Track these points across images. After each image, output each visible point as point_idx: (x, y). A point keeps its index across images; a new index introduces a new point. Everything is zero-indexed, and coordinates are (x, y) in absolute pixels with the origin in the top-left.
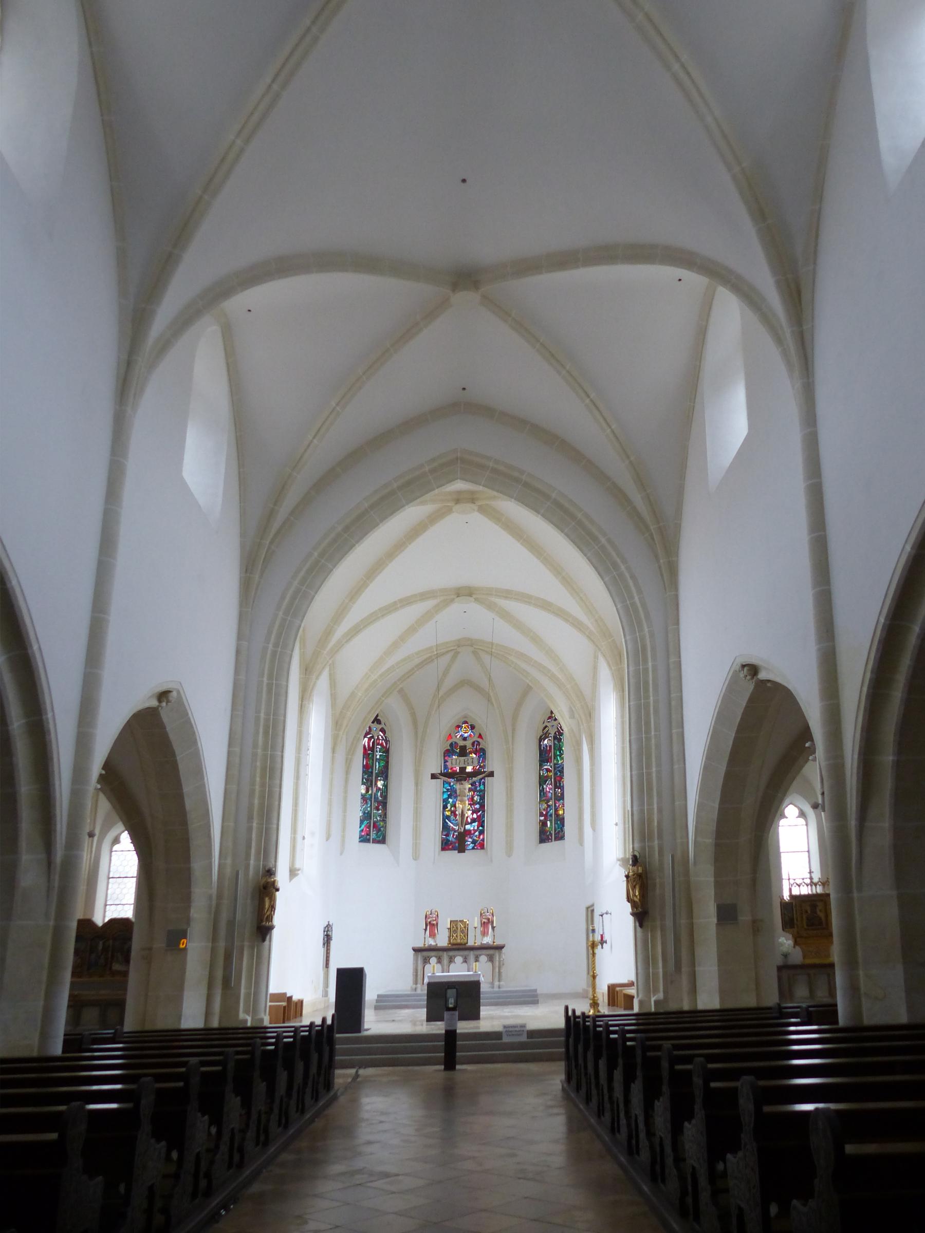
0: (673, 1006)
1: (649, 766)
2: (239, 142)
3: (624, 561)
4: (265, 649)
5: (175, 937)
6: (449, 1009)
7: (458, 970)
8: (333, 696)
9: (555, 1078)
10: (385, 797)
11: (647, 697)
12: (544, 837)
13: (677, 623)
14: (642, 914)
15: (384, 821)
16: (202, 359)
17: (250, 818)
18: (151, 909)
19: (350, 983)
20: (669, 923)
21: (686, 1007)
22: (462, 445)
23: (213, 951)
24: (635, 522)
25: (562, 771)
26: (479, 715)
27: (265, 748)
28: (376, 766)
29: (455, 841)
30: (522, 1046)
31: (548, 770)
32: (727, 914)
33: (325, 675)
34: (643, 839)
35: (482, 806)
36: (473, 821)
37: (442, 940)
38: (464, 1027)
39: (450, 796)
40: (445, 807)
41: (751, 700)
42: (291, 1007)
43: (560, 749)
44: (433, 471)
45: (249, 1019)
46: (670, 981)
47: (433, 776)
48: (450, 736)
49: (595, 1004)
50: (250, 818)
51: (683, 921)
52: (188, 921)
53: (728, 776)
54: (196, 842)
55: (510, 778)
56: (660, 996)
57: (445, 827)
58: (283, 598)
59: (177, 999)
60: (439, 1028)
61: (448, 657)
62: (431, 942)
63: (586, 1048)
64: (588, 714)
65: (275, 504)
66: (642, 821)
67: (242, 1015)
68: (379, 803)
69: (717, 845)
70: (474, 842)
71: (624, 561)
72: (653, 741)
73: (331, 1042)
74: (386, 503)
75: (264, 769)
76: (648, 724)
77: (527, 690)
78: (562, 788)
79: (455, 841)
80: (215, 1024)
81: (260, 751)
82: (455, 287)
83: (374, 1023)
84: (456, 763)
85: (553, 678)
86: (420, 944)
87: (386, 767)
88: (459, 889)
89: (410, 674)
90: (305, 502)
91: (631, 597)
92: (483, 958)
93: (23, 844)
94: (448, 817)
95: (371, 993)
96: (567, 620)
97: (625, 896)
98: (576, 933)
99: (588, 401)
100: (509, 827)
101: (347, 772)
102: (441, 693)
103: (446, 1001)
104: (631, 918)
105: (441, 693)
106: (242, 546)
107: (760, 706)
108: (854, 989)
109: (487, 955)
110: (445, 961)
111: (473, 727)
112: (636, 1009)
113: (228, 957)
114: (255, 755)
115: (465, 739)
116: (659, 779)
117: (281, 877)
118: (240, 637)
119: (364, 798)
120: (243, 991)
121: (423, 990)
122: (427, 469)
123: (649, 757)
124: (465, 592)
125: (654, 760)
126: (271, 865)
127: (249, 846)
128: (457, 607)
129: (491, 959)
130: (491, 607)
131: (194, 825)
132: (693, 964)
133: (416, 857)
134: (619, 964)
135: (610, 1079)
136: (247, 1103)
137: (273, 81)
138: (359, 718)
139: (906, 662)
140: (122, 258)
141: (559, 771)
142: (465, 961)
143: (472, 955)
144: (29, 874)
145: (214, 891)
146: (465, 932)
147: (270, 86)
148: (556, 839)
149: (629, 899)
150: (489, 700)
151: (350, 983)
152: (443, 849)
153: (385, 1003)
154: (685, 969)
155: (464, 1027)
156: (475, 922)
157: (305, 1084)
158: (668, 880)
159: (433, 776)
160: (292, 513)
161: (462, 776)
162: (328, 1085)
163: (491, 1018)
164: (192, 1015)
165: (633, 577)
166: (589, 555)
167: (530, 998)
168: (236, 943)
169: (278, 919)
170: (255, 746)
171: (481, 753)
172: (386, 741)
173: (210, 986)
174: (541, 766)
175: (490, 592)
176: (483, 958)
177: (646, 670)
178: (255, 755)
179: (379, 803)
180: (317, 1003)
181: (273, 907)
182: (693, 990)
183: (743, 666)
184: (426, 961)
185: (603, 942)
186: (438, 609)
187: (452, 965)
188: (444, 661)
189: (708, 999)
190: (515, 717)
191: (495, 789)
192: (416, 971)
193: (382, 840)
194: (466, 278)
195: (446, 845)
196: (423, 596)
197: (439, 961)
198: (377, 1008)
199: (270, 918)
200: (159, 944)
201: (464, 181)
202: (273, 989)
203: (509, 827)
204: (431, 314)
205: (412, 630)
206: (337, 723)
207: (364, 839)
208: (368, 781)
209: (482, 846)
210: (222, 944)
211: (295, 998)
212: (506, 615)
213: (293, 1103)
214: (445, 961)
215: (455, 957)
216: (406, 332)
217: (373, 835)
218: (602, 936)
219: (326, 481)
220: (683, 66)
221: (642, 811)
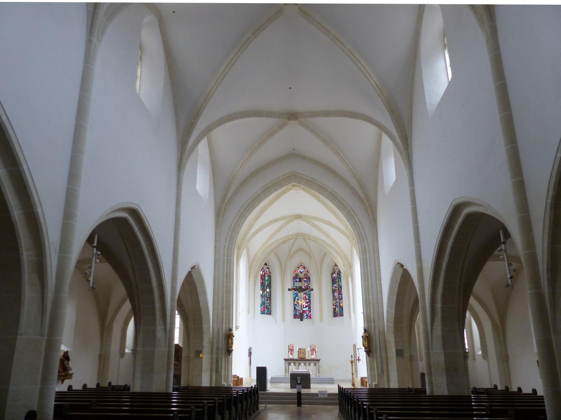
0: (381, 387)
1: (369, 295)
3: (357, 216)
5: (198, 353)
6: (298, 384)
7: (302, 369)
8: (248, 256)
9: (335, 410)
10: (270, 296)
11: (367, 269)
12: (335, 315)
13: (377, 241)
14: (369, 352)
15: (270, 305)
16: (202, 148)
17: (223, 309)
18: (189, 341)
19: (262, 372)
20: (378, 355)
21: (386, 387)
22: (294, 169)
23: (212, 358)
24: (360, 203)
25: (341, 288)
26: (306, 263)
27: (227, 283)
28: (266, 283)
29: (299, 315)
30: (326, 399)
31: (336, 287)
32: (399, 353)
33: (245, 251)
34: (368, 323)
35: (310, 301)
36: (306, 306)
37: (295, 356)
38: (304, 391)
39: (296, 296)
40: (294, 301)
42: (239, 381)
43: (340, 279)
46: (380, 378)
47: (289, 290)
48: (295, 271)
49: (353, 385)
50: (223, 309)
51: (384, 355)
52: (202, 347)
54: (204, 318)
55: (320, 289)
56: (376, 383)
57: (295, 309)
58: (230, 227)
59: (200, 376)
60: (295, 391)
61: (293, 240)
62: (291, 357)
64: (350, 266)
65: (227, 192)
66: (367, 316)
67: (223, 383)
68: (268, 298)
69: (395, 327)
70: (307, 315)
71: (357, 216)
73: (257, 394)
74: (266, 191)
75: (227, 291)
77: (325, 254)
78: (341, 295)
79: (299, 315)
80: (214, 385)
81: (225, 284)
82: (289, 119)
83: (271, 388)
84: (298, 284)
85: (335, 250)
86: (287, 358)
87: (270, 284)
88: (302, 335)
89: (278, 246)
90: (237, 190)
91: (360, 230)
92: (312, 364)
93: (158, 322)
94: (296, 305)
95: (269, 377)
98: (343, 357)
100: (321, 310)
101: (255, 285)
102: (291, 253)
103: (297, 381)
104: (365, 353)
105: (291, 253)
106: (215, 207)
107: (403, 280)
108: (431, 383)
110: (297, 364)
111: (304, 268)
112: (368, 387)
113: (217, 361)
114: (223, 285)
115: (301, 273)
116: (373, 300)
117: (234, 332)
118: (216, 241)
119: (262, 296)
120: (223, 374)
121: (288, 376)
122: (282, 178)
123: (369, 292)
124: (298, 217)
128: (296, 222)
129: (315, 364)
130: (309, 223)
131: (203, 312)
132: (388, 371)
133: (284, 320)
134: (363, 371)
136: (230, 414)
138: (259, 264)
140: (177, 123)
141: (340, 288)
142: (305, 365)
143: (307, 363)
144: (160, 334)
146: (304, 353)
148: (340, 316)
150: (310, 256)
151: (262, 372)
152: (294, 318)
153: (275, 380)
154: (385, 373)
155: (304, 391)
156: (308, 349)
157: (251, 407)
158: (377, 339)
159: (289, 290)
160: (233, 195)
161: (300, 289)
162: (257, 408)
163: (315, 388)
164: (205, 382)
165: (360, 222)
167: (331, 381)
168: (220, 356)
169: (234, 347)
170: (223, 282)
171: (308, 279)
172: (270, 273)
173: (211, 372)
174: (333, 285)
175: (308, 217)
176: (312, 364)
177: (366, 258)
178: (223, 285)
179: (268, 298)
180: (249, 380)
181: (232, 343)
182: (389, 381)
183: (398, 263)
184: (289, 364)
185: (359, 360)
186: (288, 223)
188: (291, 242)
189: (394, 385)
190: (321, 264)
191: (315, 295)
192: (286, 368)
193: (270, 313)
194: (292, 116)
195: (295, 316)
196: (282, 218)
197: (295, 364)
198: (271, 382)
199: (231, 347)
200: (192, 355)
202: (233, 374)
203: (321, 310)
204: (281, 127)
205: (278, 230)
206: (250, 267)
207: (263, 313)
208: (263, 289)
209: (310, 317)
210: (215, 356)
211: (240, 377)
212: (315, 226)
213: (248, 412)
214: (297, 364)
216: (272, 133)
217: (266, 311)
219: (244, 182)
220: (362, 65)
221: (367, 312)
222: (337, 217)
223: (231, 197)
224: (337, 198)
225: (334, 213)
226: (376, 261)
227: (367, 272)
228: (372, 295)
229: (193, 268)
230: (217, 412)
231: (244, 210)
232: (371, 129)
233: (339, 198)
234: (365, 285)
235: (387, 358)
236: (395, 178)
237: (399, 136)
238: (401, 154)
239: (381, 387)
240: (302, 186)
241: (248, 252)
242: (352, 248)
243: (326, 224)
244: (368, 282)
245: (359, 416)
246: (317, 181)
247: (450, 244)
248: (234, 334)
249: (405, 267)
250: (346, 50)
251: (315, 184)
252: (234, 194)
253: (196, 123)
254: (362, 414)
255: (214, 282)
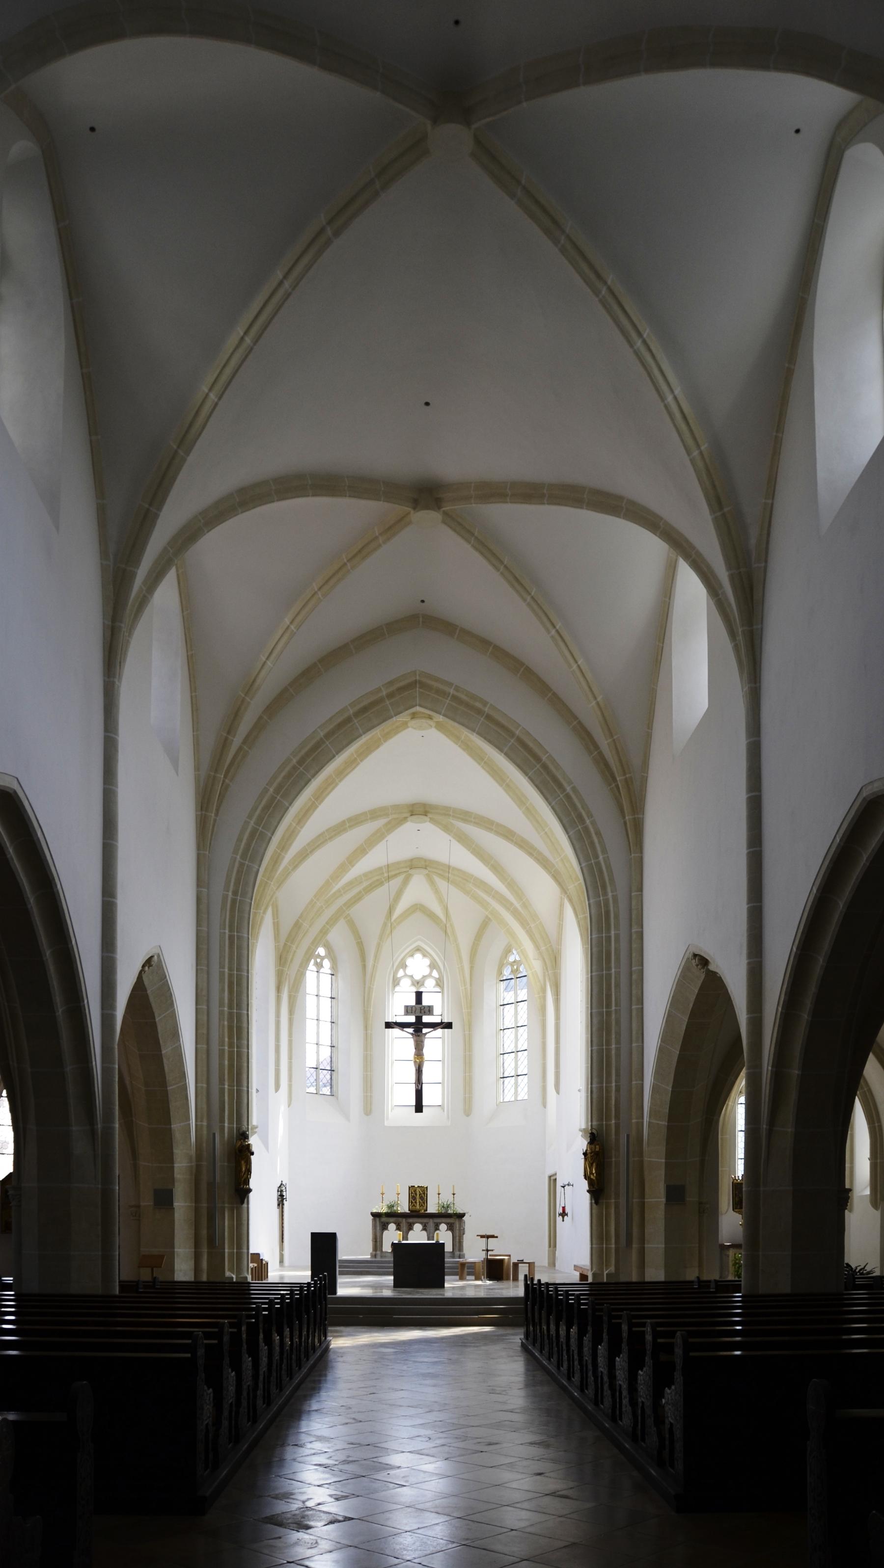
1: (608, 1043)
2: (213, 396)
4: (225, 897)
7: (418, 1236)
8: (276, 926)
11: (609, 968)
13: (640, 889)
14: (598, 1190)
16: (166, 596)
17: (221, 1081)
20: (623, 1200)
23: (197, 1210)
32: (675, 1195)
34: (600, 1119)
41: (702, 988)
44: (390, 696)
45: (234, 1276)
50: (221, 1081)
52: (172, 1180)
53: (681, 1059)
54: (174, 1105)
56: (612, 1269)
63: (541, 1315)
65: (229, 732)
67: (228, 1274)
72: (613, 1016)
76: (609, 997)
80: (204, 1278)
83: (347, 1287)
90: (259, 727)
96: (530, 854)
97: (583, 1173)
99: (553, 632)
104: (588, 1195)
106: (197, 779)
109: (447, 1224)
116: (618, 1055)
117: (254, 1141)
124: (420, 810)
125: (613, 1036)
126: (244, 1129)
127: (222, 1110)
128: (410, 827)
129: (451, 1228)
132: (642, 1240)
135: (540, 1314)
137: (246, 333)
139: (812, 989)
143: (431, 1223)
145: (193, 1152)
147: (242, 339)
149: (586, 1177)
151: (323, 1246)
153: (358, 1268)
154: (635, 1246)
160: (245, 742)
166: (553, 803)
169: (253, 1183)
177: (609, 939)
181: (249, 1171)
183: (695, 955)
184: (385, 1227)
185: (564, 1214)
186: (392, 826)
187: (411, 1232)
189: (655, 1273)
194: (427, 494)
196: (374, 814)
200: (147, 1202)
201: (427, 404)
204: (392, 529)
207: (424, 1190)
212: (464, 840)
215: (414, 1224)
216: (362, 549)
218: (564, 1208)
220: (645, 342)
222: (530, 812)
223: (240, 749)
224: (538, 759)
225: (520, 800)
226: (634, 946)
227: (609, 976)
228: (618, 1042)
229: (148, 962)
230: (274, 1328)
231: (277, 791)
232: (651, 548)
233: (544, 758)
234: (600, 1014)
235: (642, 1205)
236: (706, 706)
237: (732, 578)
238: (732, 634)
239: (623, 1278)
240: (440, 718)
241: (276, 915)
242: (562, 906)
243: (498, 833)
244: (609, 1005)
245: (597, 1341)
246: (485, 703)
247: (841, 905)
248: (254, 1149)
249: (712, 967)
250: (604, 291)
251: (479, 712)
252: (250, 739)
253: (156, 516)
254: (605, 1336)
255: (197, 1004)
